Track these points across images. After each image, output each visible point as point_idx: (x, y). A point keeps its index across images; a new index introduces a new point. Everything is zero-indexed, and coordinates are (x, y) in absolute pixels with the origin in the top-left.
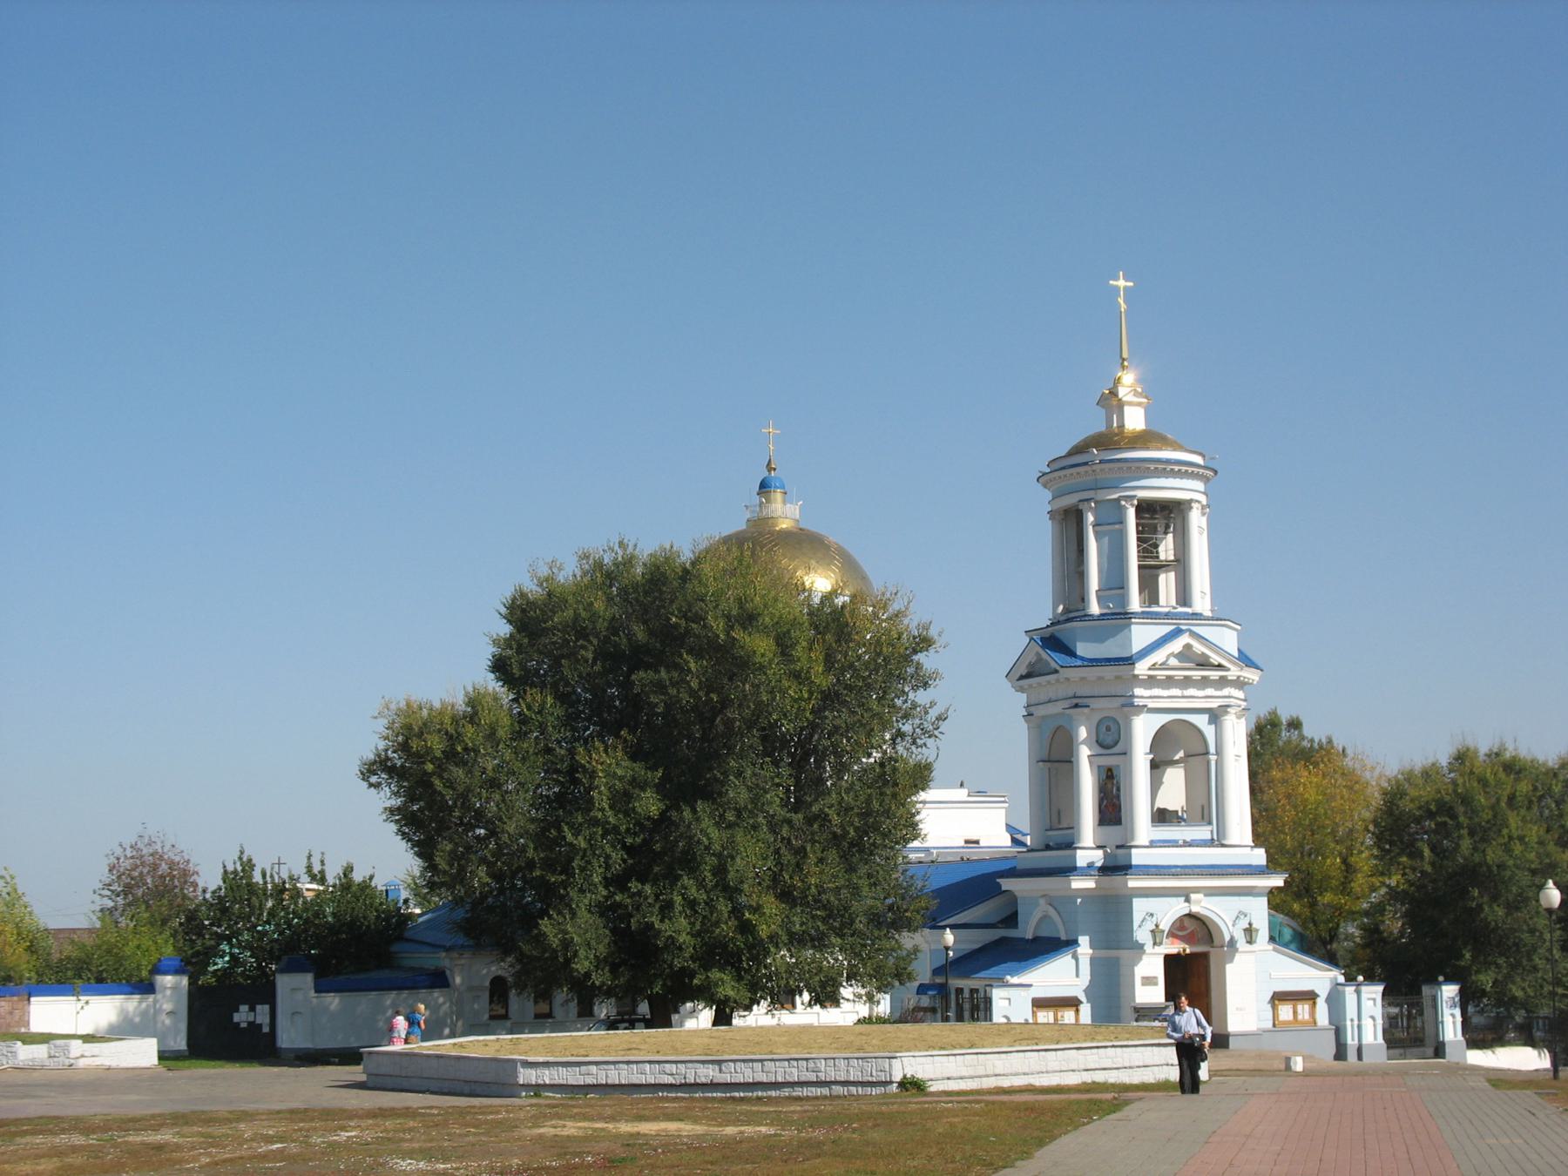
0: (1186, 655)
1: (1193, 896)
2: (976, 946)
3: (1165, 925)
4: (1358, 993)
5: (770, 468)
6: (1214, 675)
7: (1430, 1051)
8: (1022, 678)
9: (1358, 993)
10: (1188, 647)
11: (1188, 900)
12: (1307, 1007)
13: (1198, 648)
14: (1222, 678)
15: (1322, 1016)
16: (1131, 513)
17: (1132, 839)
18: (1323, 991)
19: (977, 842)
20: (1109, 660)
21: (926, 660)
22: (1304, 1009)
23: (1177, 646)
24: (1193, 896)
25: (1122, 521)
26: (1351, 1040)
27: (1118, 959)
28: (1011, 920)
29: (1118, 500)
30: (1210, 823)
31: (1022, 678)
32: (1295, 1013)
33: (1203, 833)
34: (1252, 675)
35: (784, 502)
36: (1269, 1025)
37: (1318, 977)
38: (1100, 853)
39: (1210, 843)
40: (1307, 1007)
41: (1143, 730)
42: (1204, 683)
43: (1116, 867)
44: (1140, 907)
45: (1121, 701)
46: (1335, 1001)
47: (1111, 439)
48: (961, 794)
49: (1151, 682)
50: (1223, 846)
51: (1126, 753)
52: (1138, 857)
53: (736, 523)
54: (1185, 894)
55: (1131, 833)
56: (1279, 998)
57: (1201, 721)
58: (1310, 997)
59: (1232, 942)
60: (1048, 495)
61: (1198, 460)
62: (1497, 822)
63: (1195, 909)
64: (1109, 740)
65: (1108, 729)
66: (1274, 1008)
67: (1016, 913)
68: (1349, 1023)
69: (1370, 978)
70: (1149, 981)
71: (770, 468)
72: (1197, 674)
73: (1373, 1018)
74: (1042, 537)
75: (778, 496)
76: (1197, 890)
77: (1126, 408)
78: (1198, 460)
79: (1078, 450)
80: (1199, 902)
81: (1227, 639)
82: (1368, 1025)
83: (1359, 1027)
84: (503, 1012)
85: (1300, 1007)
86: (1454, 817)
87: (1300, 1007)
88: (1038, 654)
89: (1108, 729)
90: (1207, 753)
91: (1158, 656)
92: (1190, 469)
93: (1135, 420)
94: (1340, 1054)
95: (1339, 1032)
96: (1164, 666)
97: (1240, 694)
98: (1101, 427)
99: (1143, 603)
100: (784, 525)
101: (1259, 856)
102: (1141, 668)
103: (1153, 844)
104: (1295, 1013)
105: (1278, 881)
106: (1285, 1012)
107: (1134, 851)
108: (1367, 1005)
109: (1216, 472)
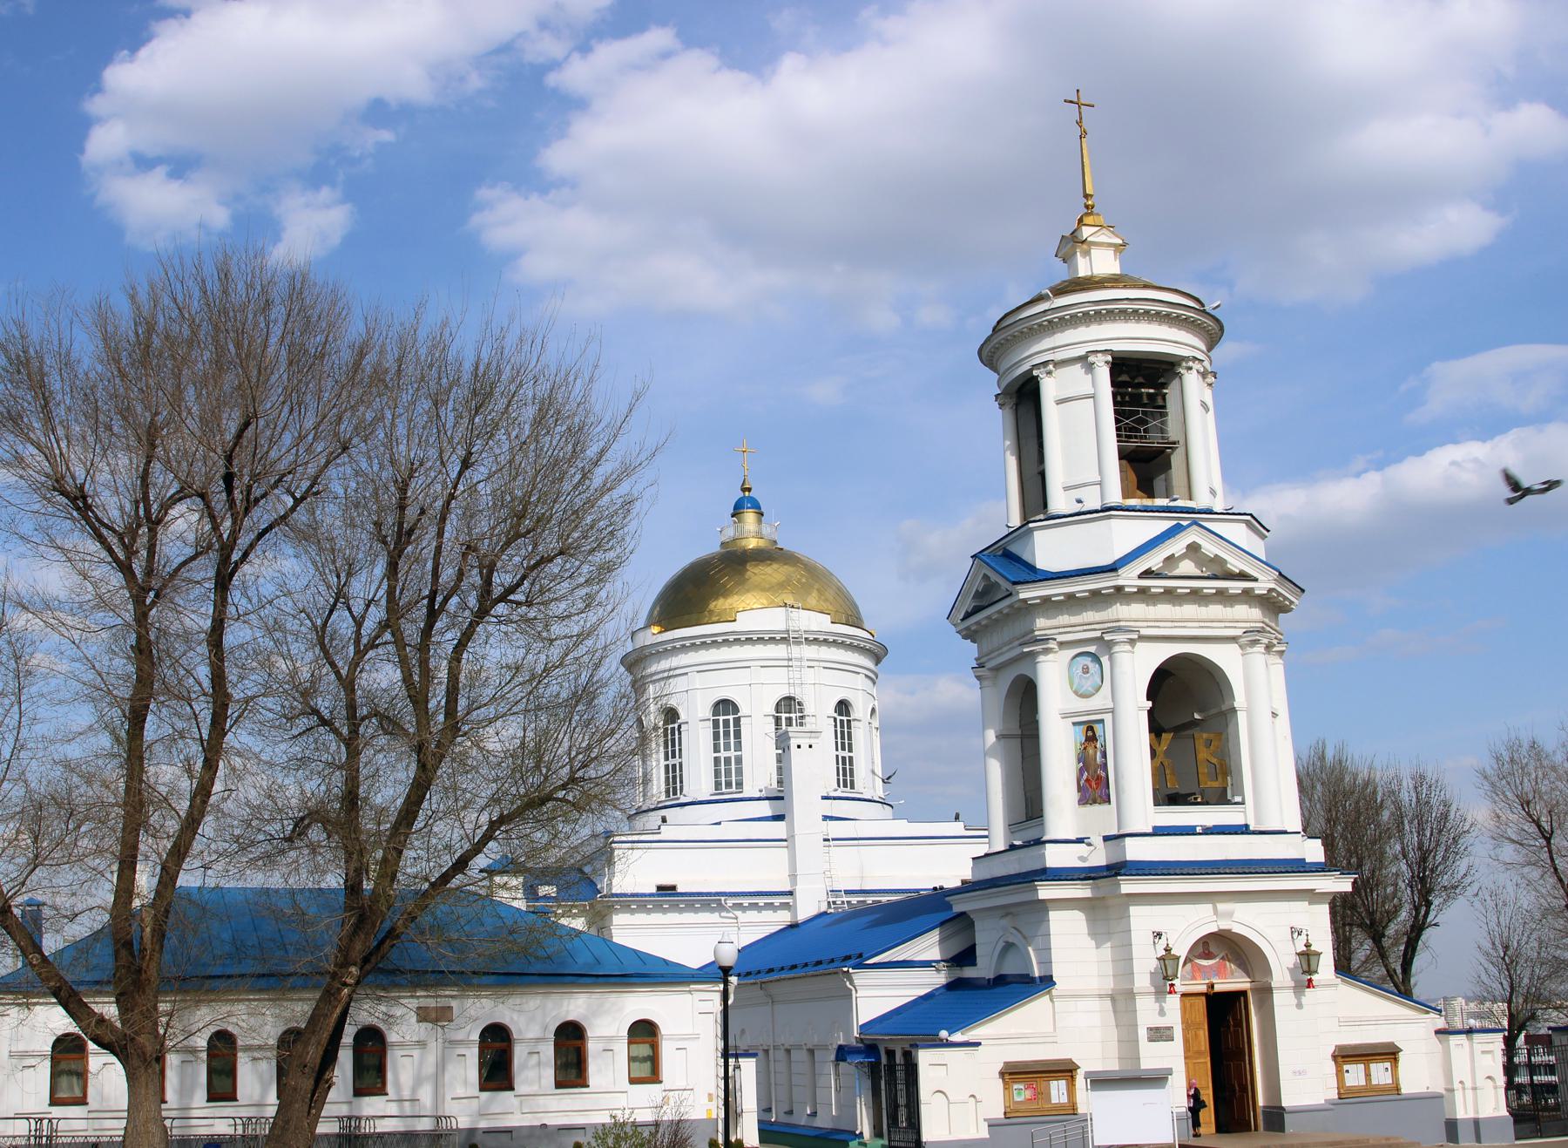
2: (922, 992)
3: (1181, 950)
5: (744, 490)
6: (1235, 587)
8: (967, 616)
12: (1063, 1083)
13: (1210, 548)
14: (1246, 592)
19: (674, 888)
23: (1177, 546)
32: (1368, 1075)
40: (1063, 1083)
42: (1222, 597)
48: (957, 828)
56: (1344, 1056)
66: (1006, 1086)
72: (1210, 586)
74: (992, 423)
84: (78, 1093)
88: (986, 577)
99: (1124, 497)
101: (1314, 851)
103: (1158, 832)
104: (1368, 1075)
105: (1344, 885)
106: (1355, 1075)
109: (1213, 332)
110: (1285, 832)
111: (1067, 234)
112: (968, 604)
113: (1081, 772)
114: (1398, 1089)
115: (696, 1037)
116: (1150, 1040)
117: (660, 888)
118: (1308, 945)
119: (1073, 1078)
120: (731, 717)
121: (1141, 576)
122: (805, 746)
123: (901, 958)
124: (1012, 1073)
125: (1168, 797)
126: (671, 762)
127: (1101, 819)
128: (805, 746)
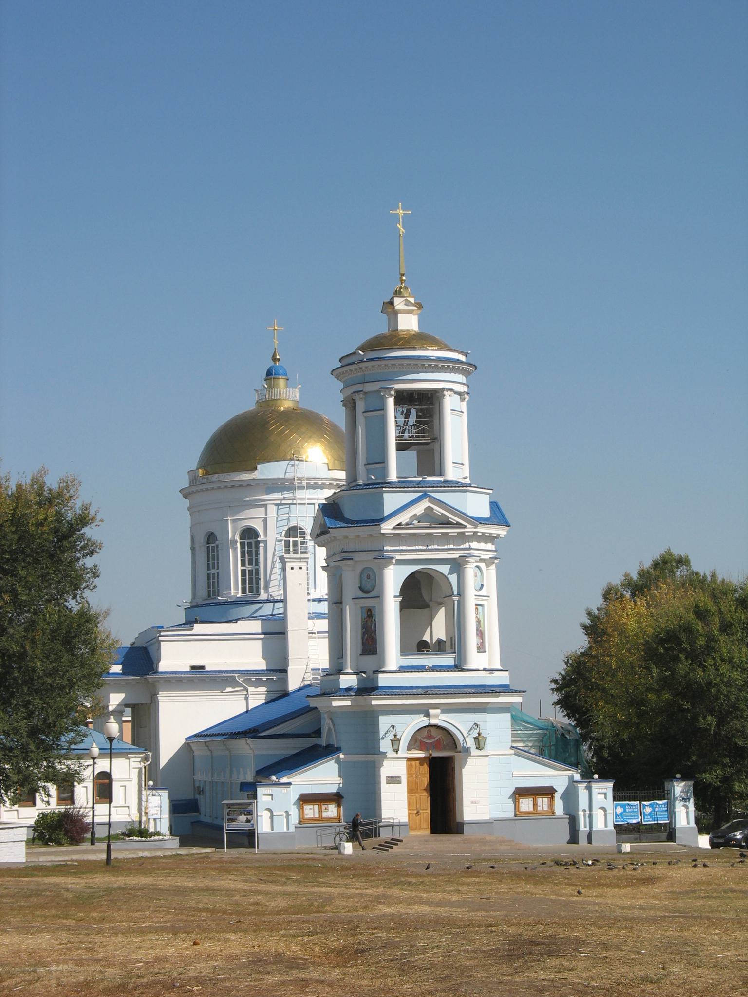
0: (429, 517)
1: (431, 712)
4: (589, 789)
5: (275, 359)
7: (664, 835)
8: (318, 535)
9: (589, 789)
10: (429, 509)
11: (427, 715)
12: (546, 800)
13: (438, 510)
15: (559, 808)
16: (391, 402)
17: (384, 666)
18: (561, 787)
19: (203, 667)
20: (358, 522)
21: (88, 532)
22: (543, 803)
24: (431, 712)
25: (383, 409)
26: (582, 827)
27: (374, 762)
28: (318, 733)
29: (379, 392)
30: (454, 653)
31: (318, 535)
33: (448, 660)
34: (502, 531)
35: (287, 386)
36: (511, 814)
37: (558, 777)
38: (355, 677)
39: (458, 667)
41: (393, 579)
43: (368, 688)
44: (385, 722)
45: (376, 553)
46: (570, 796)
47: (394, 339)
49: (397, 538)
50: (463, 670)
51: (380, 597)
52: (384, 680)
53: (247, 405)
54: (425, 711)
55: (382, 662)
56: (521, 793)
57: (444, 569)
58: (549, 792)
59: (467, 750)
60: (341, 385)
61: (463, 358)
62: (710, 648)
63: (434, 721)
64: (368, 586)
65: (369, 577)
67: (320, 729)
68: (581, 813)
69: (604, 777)
70: (394, 780)
71: (275, 359)
73: (603, 809)
75: (282, 382)
76: (435, 706)
77: (399, 315)
78: (463, 358)
79: (368, 346)
80: (437, 716)
81: (478, 504)
82: (598, 815)
83: (590, 816)
85: (539, 800)
86: (679, 644)
87: (539, 800)
89: (369, 577)
90: (452, 595)
91: (404, 518)
92: (452, 365)
93: (408, 323)
94: (574, 839)
95: (573, 821)
96: (408, 526)
97: (490, 546)
98: (384, 330)
100: (286, 405)
102: (387, 528)
103: (403, 669)
104: (535, 805)
106: (526, 804)
107: (380, 675)
108: (598, 799)
110: (478, 670)
111: (186, 484)
112: (318, 531)
113: (364, 634)
114: (553, 813)
115: (130, 780)
116: (388, 783)
117: (193, 668)
118: (479, 734)
119: (553, 798)
120: (253, 541)
121: (394, 528)
122: (296, 568)
123: (282, 732)
124: (305, 799)
125: (405, 650)
126: (212, 571)
127: (369, 662)
128: (296, 568)
